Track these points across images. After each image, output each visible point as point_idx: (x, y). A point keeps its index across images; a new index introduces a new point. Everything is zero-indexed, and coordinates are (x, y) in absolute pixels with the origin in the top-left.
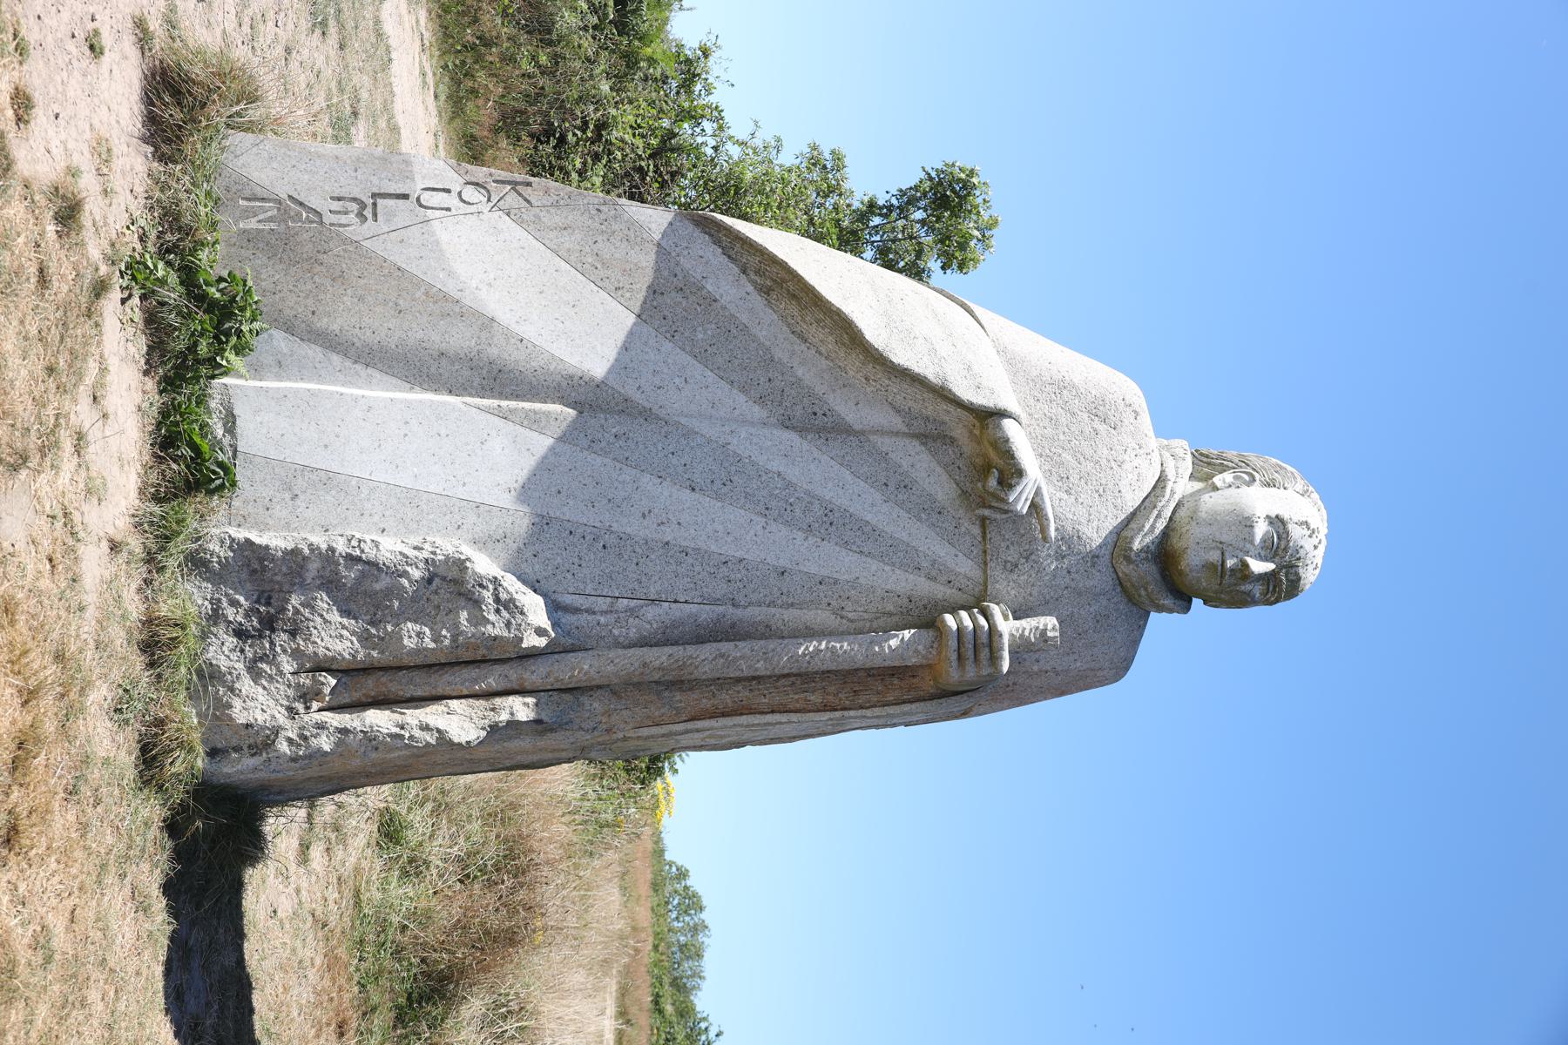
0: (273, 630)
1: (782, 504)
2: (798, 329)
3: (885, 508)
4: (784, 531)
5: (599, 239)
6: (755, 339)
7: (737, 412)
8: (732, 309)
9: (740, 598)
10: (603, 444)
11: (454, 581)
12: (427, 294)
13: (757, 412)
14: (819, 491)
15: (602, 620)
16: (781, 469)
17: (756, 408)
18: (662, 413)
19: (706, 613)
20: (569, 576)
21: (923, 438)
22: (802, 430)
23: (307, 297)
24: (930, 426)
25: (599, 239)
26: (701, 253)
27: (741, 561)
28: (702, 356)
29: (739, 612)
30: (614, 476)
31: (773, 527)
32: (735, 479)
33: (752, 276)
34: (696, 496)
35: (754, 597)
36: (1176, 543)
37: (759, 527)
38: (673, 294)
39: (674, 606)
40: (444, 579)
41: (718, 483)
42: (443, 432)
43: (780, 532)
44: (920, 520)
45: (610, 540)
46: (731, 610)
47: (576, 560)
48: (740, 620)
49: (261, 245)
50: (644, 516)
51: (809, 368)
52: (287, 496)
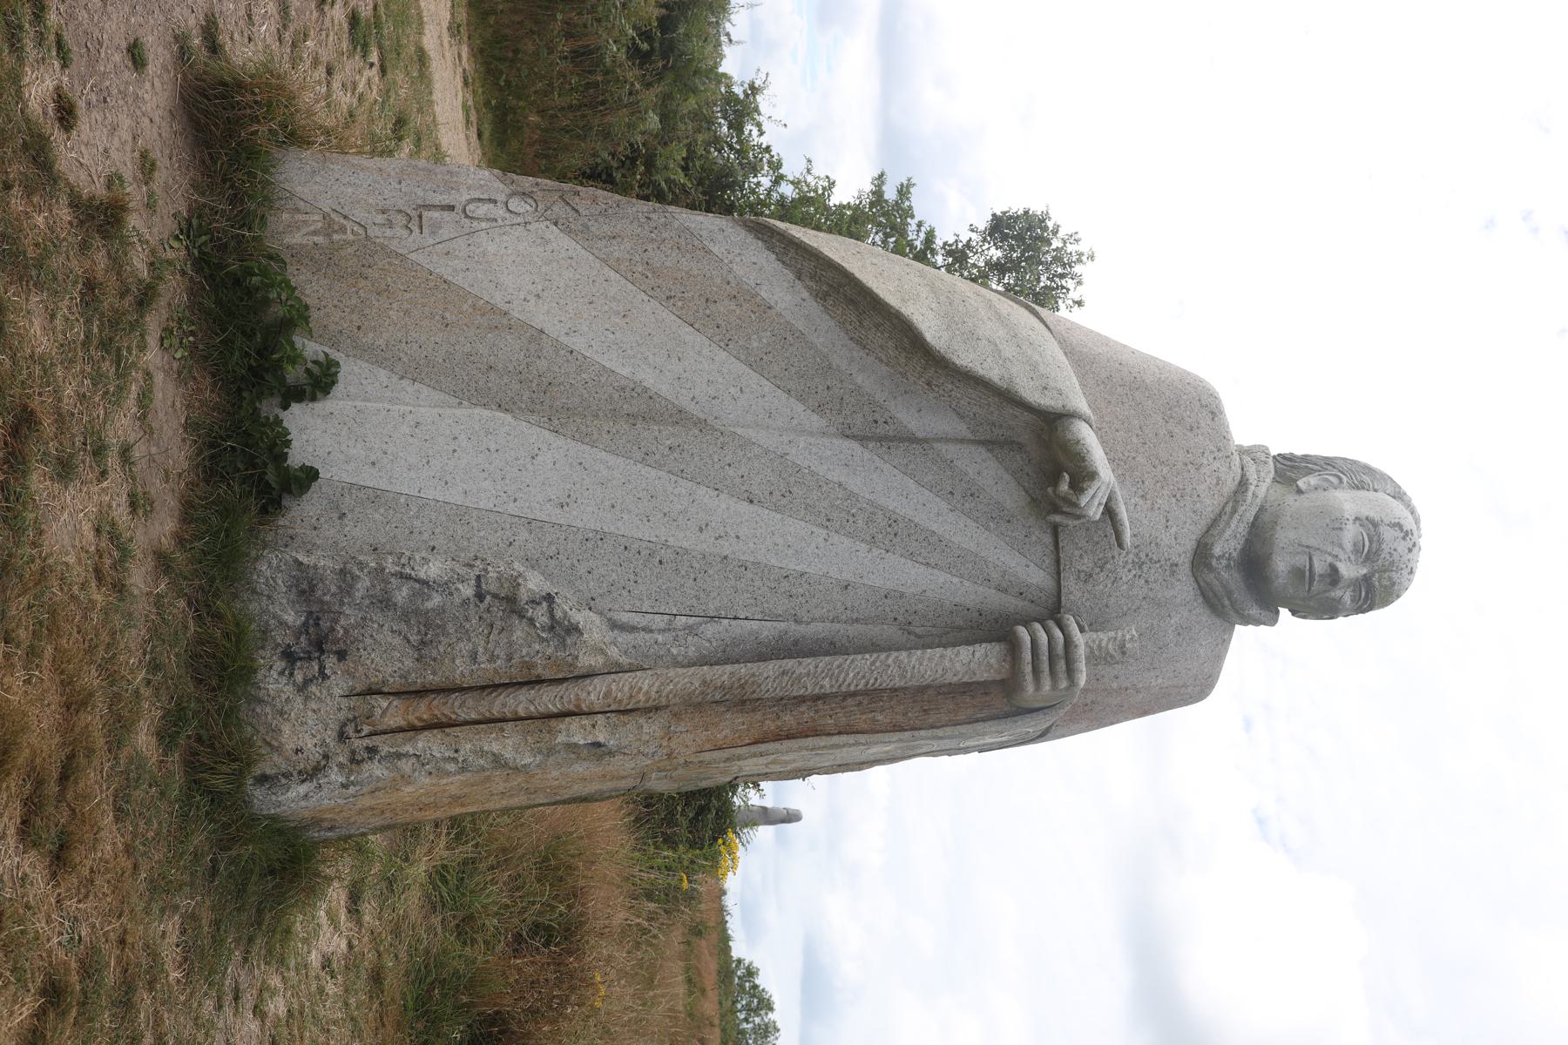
0: (322, 652)
1: (843, 514)
3: (951, 517)
4: (847, 542)
7: (795, 422)
9: (802, 614)
10: (658, 457)
12: (474, 306)
13: (816, 422)
17: (815, 417)
19: (768, 630)
20: (625, 593)
21: (989, 444)
22: (862, 439)
23: (352, 312)
26: (754, 259)
27: (802, 575)
29: (802, 628)
31: (835, 538)
34: (752, 508)
35: (817, 613)
38: (726, 302)
39: (734, 623)
40: (495, 596)
41: (777, 494)
42: (493, 447)
43: (842, 543)
46: (793, 626)
47: (632, 577)
50: (701, 530)
51: (866, 375)
52: (335, 515)
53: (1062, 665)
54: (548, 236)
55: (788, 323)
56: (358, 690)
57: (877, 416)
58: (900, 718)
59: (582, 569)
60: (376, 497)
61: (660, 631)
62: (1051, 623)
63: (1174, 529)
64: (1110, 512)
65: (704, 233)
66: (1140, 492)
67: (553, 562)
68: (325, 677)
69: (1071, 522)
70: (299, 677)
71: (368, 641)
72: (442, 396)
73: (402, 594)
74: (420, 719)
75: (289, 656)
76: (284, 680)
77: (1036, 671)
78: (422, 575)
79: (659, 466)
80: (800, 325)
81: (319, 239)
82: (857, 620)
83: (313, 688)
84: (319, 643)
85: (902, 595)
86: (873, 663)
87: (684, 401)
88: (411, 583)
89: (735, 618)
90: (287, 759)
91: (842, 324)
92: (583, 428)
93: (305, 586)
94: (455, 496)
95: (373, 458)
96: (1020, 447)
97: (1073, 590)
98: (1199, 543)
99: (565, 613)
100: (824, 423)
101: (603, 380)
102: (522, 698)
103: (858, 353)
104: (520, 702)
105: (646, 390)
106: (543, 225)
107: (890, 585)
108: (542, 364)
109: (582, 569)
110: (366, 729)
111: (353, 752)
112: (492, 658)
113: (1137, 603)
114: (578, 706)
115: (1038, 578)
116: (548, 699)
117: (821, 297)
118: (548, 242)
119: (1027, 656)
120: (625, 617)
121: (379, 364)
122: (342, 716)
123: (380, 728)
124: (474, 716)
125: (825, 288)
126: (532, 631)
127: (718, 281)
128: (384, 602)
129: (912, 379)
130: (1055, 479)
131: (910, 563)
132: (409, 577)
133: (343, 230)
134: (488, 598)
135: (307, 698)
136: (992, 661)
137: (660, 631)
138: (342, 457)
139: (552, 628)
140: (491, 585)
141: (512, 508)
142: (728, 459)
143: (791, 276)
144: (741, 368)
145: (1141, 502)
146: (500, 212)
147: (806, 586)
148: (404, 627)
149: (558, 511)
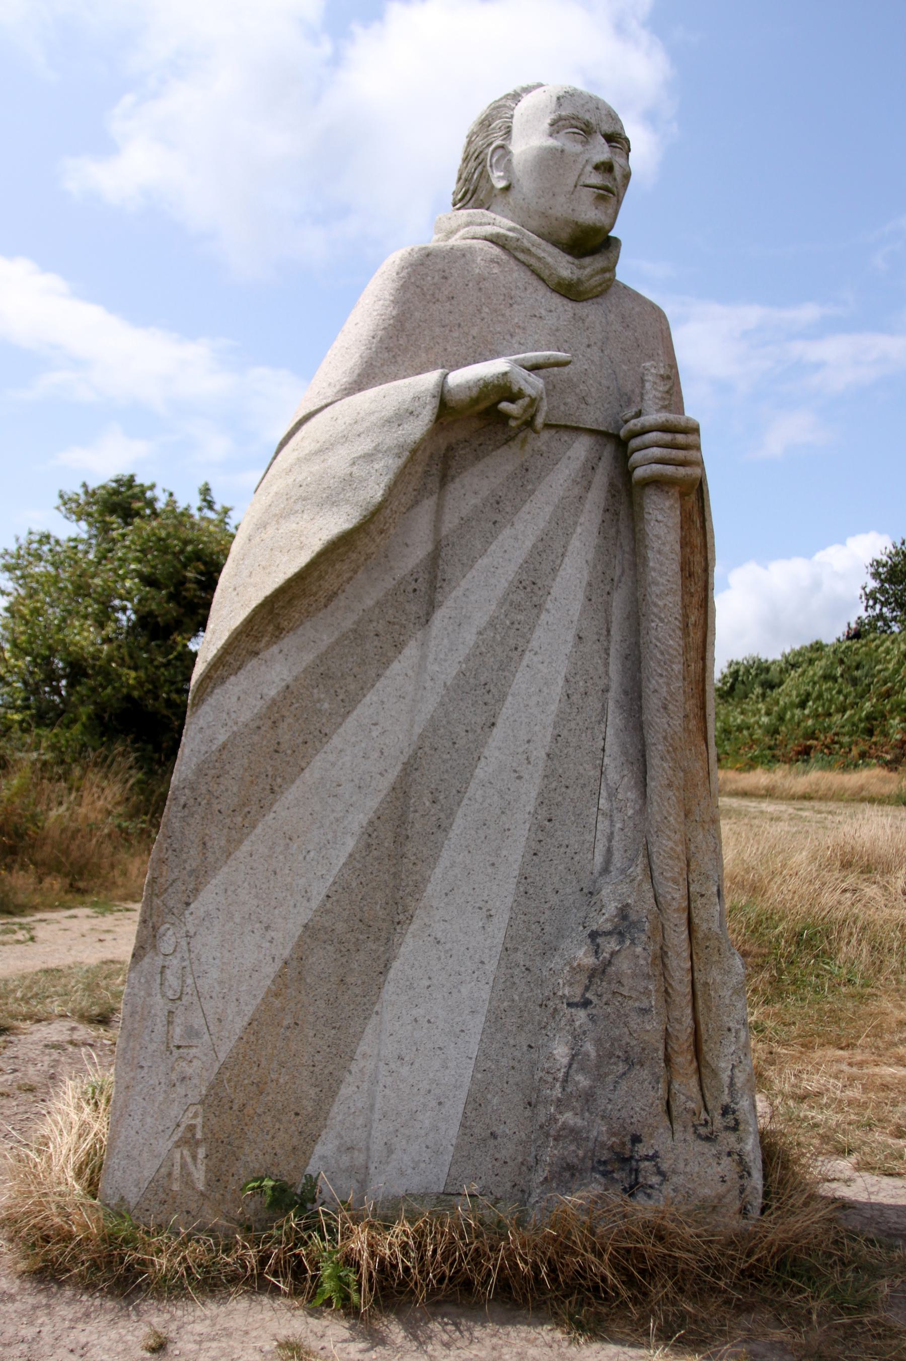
0: (632, 1157)
1: (512, 632)
2: (323, 600)
3: (519, 526)
4: (538, 632)
5: (216, 807)
6: (331, 648)
7: (410, 673)
8: (297, 670)
9: (601, 683)
10: (442, 815)
11: (591, 977)
12: (276, 995)
13: (411, 651)
14: (499, 592)
15: (618, 825)
16: (474, 631)
17: (407, 652)
18: (408, 752)
19: (615, 719)
20: (577, 858)
21: (444, 479)
22: (432, 606)
23: (279, 1121)
24: (434, 471)
25: (216, 807)
26: (234, 699)
27: (567, 681)
28: (350, 703)
29: (615, 686)
30: (477, 806)
31: (534, 644)
32: (482, 679)
33: (262, 644)
34: (500, 722)
35: (601, 669)
36: (545, 231)
37: (535, 659)
38: (280, 731)
39: (607, 752)
40: (587, 989)
41: (487, 698)
42: (427, 983)
43: (539, 637)
44: (533, 492)
45: (543, 813)
46: (611, 694)
47: (562, 850)
48: (621, 685)
49: (224, 1168)
50: (520, 778)
51: (368, 594)
52: (492, 1142)
53: (680, 438)
54: (201, 913)
55: (305, 671)
56: (668, 1123)
57: (410, 589)
58: (695, 600)
59: (554, 899)
60: (476, 1102)
61: (612, 825)
62: (635, 443)
63: (543, 312)
64: (534, 368)
65: (204, 749)
66: (508, 337)
67: (547, 928)
68: (655, 1156)
69: (544, 407)
70: (655, 1180)
71: (624, 1114)
72: (368, 1030)
73: (582, 1081)
74: (691, 1062)
75: (631, 1190)
76: (655, 1193)
77: (683, 464)
78: (565, 1061)
79: (451, 815)
80: (308, 658)
81: (201, 1152)
82: (608, 631)
83: (664, 1167)
84: (623, 1163)
85: (590, 584)
86: (661, 620)
87: (385, 784)
88: (572, 1072)
89: (603, 750)
90: (729, 1191)
91: (309, 615)
92: (408, 890)
93: (567, 1175)
94: (477, 1024)
95: (434, 1103)
96: (450, 448)
97: (593, 417)
98: (553, 290)
99: (607, 920)
100: (412, 643)
101: (358, 866)
102: (675, 964)
103: (341, 601)
104: (679, 964)
105: (371, 823)
106: (190, 919)
107: (581, 596)
108: (340, 927)
109: (554, 899)
110: (703, 1115)
111: (727, 1128)
112: (646, 992)
113: (606, 359)
114: (684, 909)
115: (581, 449)
116: (678, 938)
117: (279, 633)
118: (208, 914)
119: (669, 470)
120: (599, 859)
121: (334, 1094)
122: (690, 1136)
123: (701, 1103)
124: (689, 1011)
125: (271, 628)
126: (623, 953)
127: (256, 738)
128: (588, 1097)
129: (373, 549)
130: (505, 417)
131: (561, 573)
132: (567, 1074)
133: (191, 1128)
134: (588, 995)
135: (674, 1172)
136: (667, 504)
137: (612, 825)
138: (431, 1135)
139: (621, 934)
140: (575, 992)
141: (491, 967)
142: (448, 744)
143: (254, 662)
144: (350, 723)
145: (517, 338)
146: (175, 962)
147: (578, 677)
148: (610, 1079)
149: (495, 920)
